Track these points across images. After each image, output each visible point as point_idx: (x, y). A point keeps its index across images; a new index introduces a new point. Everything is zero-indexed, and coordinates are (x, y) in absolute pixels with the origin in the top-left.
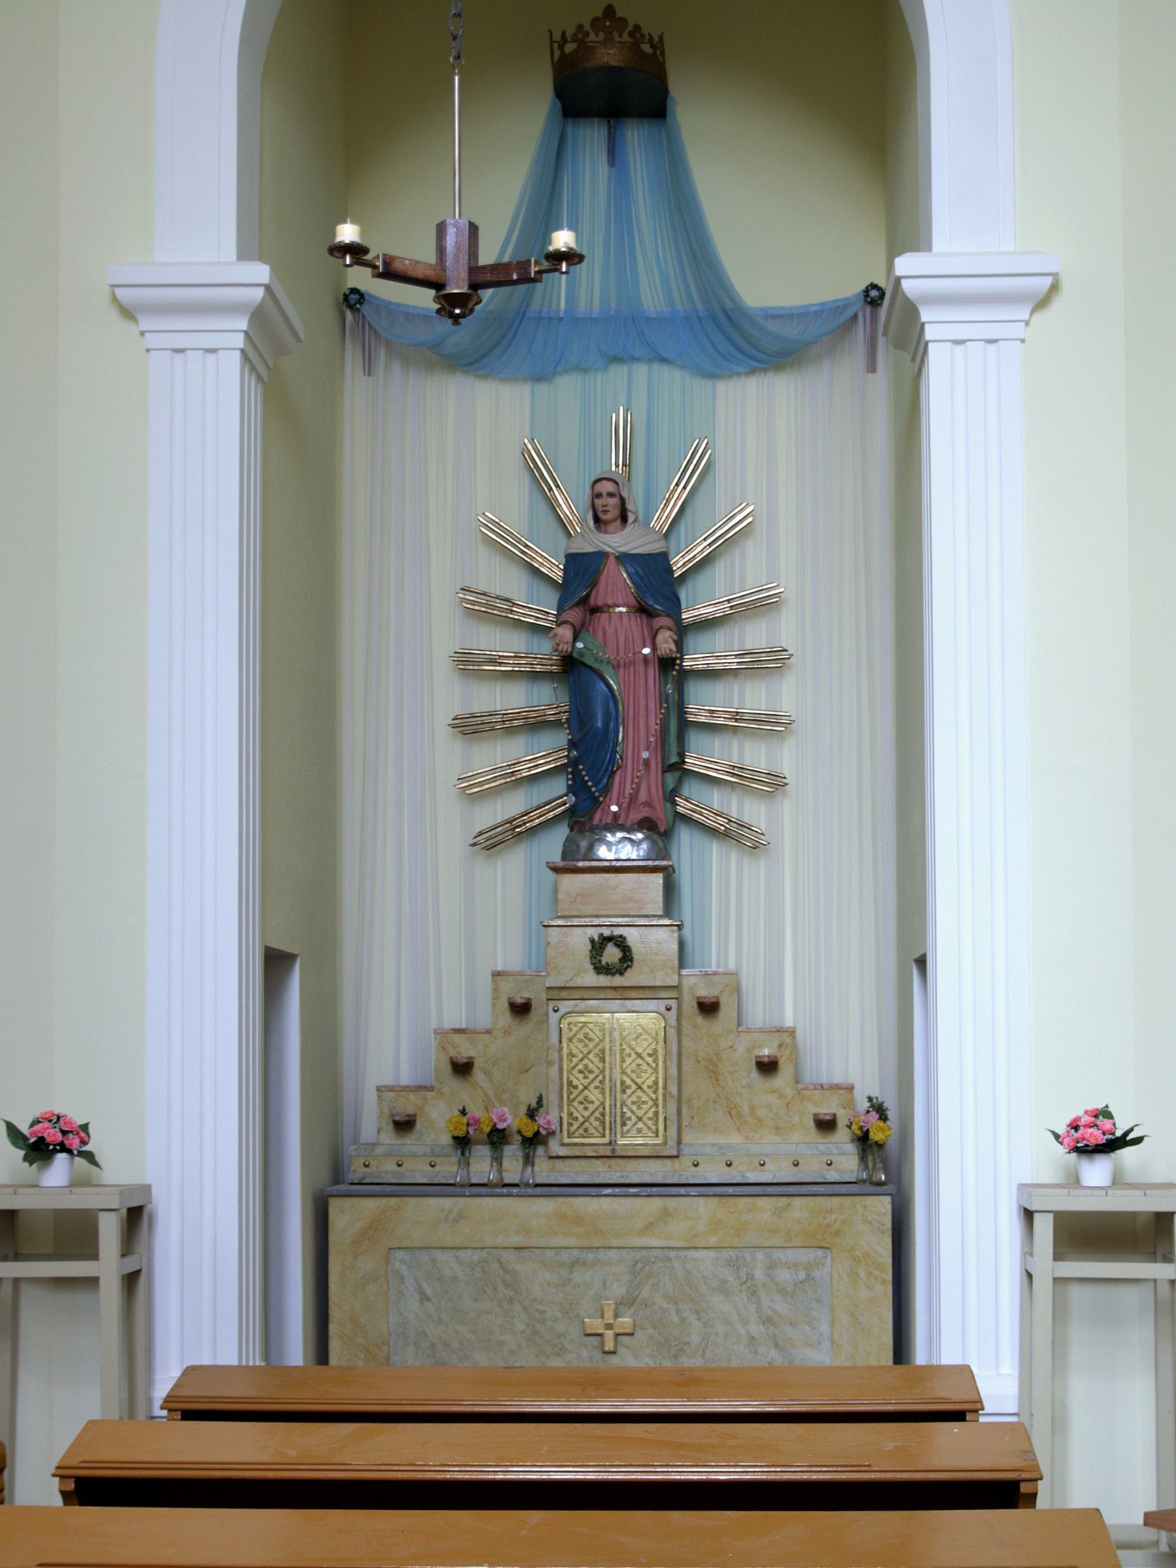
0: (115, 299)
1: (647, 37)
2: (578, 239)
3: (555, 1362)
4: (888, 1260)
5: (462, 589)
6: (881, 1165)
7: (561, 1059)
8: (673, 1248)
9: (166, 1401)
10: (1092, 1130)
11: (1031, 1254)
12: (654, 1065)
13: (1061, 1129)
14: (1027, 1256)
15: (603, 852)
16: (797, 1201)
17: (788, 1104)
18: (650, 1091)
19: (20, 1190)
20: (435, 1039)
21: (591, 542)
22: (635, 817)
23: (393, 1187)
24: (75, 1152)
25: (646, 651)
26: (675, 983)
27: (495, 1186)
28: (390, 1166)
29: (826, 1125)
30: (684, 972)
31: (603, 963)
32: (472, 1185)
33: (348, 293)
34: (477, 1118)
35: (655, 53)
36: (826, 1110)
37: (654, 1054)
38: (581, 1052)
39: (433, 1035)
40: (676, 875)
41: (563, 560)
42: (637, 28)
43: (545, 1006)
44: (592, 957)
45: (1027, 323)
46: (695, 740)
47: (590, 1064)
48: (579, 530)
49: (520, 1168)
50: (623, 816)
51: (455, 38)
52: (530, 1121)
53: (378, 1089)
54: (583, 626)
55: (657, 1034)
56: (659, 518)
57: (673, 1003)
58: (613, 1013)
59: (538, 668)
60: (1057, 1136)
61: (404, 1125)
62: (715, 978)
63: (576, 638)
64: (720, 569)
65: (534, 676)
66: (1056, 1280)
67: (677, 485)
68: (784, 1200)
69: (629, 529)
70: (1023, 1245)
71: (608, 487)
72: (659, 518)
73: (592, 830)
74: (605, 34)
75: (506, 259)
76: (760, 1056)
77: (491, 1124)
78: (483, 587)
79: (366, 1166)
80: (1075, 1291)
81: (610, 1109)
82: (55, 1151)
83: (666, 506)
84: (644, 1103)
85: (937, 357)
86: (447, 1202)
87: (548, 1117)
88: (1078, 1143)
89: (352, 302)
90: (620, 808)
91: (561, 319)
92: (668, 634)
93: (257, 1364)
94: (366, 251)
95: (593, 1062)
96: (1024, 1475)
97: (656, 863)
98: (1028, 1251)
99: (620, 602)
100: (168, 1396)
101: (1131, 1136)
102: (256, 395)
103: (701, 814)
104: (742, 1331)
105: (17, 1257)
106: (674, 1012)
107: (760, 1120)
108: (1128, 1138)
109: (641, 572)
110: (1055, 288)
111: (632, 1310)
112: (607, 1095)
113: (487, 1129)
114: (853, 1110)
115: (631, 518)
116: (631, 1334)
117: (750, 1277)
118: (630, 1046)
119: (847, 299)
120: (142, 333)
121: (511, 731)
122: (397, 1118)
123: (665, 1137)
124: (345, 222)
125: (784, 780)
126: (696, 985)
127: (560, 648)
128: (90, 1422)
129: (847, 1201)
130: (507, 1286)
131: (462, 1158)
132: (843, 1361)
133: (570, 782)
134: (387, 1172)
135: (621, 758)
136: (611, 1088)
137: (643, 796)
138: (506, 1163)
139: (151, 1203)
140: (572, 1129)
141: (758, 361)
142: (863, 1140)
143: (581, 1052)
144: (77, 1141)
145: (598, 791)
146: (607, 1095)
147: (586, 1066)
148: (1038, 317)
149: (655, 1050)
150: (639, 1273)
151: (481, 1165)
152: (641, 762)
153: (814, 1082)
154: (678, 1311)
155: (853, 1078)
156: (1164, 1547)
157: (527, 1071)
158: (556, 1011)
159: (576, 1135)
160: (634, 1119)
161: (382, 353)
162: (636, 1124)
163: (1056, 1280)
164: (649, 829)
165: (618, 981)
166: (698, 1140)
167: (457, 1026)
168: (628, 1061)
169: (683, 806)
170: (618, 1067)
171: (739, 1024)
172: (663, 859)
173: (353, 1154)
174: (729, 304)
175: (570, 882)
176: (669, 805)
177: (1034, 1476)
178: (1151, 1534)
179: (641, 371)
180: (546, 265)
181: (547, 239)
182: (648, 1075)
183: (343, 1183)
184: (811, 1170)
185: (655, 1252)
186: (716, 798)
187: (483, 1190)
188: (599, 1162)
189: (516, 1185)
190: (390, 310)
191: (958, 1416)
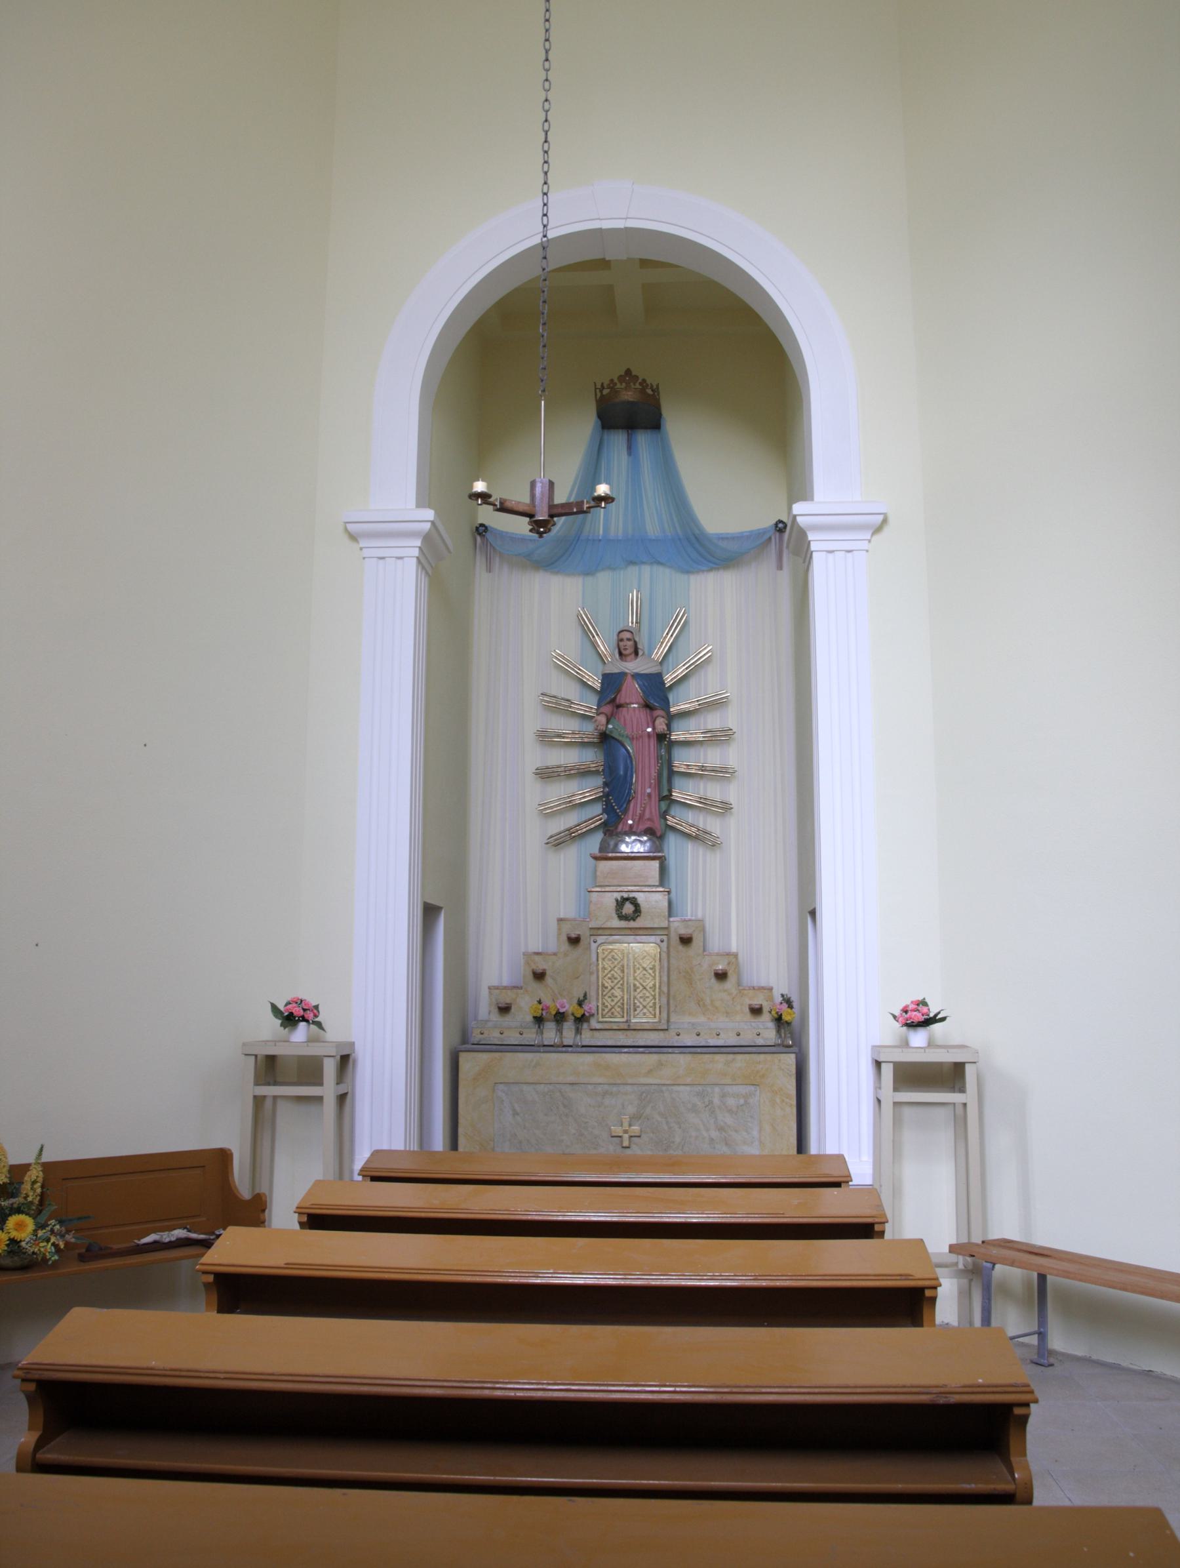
0: (346, 530)
1: (650, 385)
2: (611, 489)
3: (593, 1152)
4: (793, 1092)
5: (542, 694)
6: (789, 1035)
7: (598, 971)
8: (664, 1085)
9: (361, 1171)
10: (915, 1013)
11: (880, 1088)
12: (653, 975)
13: (897, 1013)
14: (878, 1089)
15: (623, 848)
16: (739, 1057)
17: (733, 998)
18: (651, 991)
19: (277, 1044)
20: (524, 958)
21: (617, 666)
22: (642, 827)
23: (498, 1047)
24: (311, 1022)
25: (649, 730)
26: (666, 926)
27: (558, 1046)
28: (496, 1034)
29: (756, 1011)
30: (671, 919)
31: (624, 913)
32: (544, 1046)
33: (478, 526)
34: (548, 1005)
35: (654, 394)
36: (757, 1001)
37: (653, 968)
38: (610, 966)
39: (522, 956)
40: (666, 862)
41: (601, 678)
42: (644, 381)
43: (588, 939)
44: (617, 910)
45: (869, 541)
46: (678, 782)
47: (615, 974)
48: (610, 660)
49: (573, 1036)
50: (635, 826)
51: (542, 381)
52: (579, 1007)
53: (489, 988)
54: (612, 715)
55: (655, 956)
56: (657, 653)
57: (665, 938)
58: (629, 943)
59: (586, 740)
60: (895, 1017)
61: (504, 1010)
62: (690, 923)
63: (608, 722)
64: (692, 682)
65: (583, 744)
66: (895, 1104)
67: (667, 634)
68: (731, 1056)
69: (638, 659)
70: (875, 1083)
71: (627, 635)
72: (657, 653)
73: (617, 834)
74: (626, 383)
75: (572, 500)
76: (717, 970)
77: (556, 1009)
78: (554, 693)
79: (482, 1034)
80: (907, 1112)
81: (627, 1001)
82: (299, 1021)
83: (661, 646)
84: (648, 997)
85: (818, 561)
86: (529, 1056)
87: (590, 1005)
88: (907, 1020)
89: (481, 531)
90: (633, 821)
91: (600, 540)
92: (662, 720)
93: (416, 1149)
94: (489, 496)
95: (617, 973)
96: (877, 1220)
97: (655, 854)
98: (878, 1085)
99: (634, 701)
100: (363, 1168)
101: (939, 1016)
102: (425, 583)
103: (682, 826)
104: (705, 1134)
105: (275, 1083)
106: (665, 944)
107: (717, 1008)
108: (937, 1018)
109: (646, 684)
110: (885, 521)
111: (640, 1122)
112: (625, 993)
113: (554, 1013)
114: (773, 1002)
115: (640, 653)
116: (639, 1137)
117: (711, 1102)
118: (639, 963)
119: (765, 528)
120: (361, 549)
121: (570, 776)
122: (500, 1005)
123: (660, 1018)
124: (478, 480)
125: (731, 806)
126: (678, 927)
127: (599, 728)
128: (317, 1181)
129: (769, 1057)
130: (565, 1106)
131: (539, 1030)
132: (766, 1152)
133: (604, 807)
134: (494, 1037)
135: (635, 793)
136: (627, 988)
137: (647, 815)
138: (565, 1033)
139: (354, 1052)
140: (604, 1013)
141: (715, 564)
142: (779, 1020)
143: (610, 966)
144: (312, 1015)
145: (620, 812)
146: (625, 993)
147: (613, 975)
148: (876, 538)
149: (654, 966)
150: (644, 1099)
151: (550, 1034)
152: (646, 794)
153: (749, 985)
154: (667, 1123)
155: (772, 982)
156: (961, 1266)
157: (577, 978)
158: (595, 942)
159: (607, 1016)
160: (641, 1006)
161: (497, 559)
162: (642, 1010)
163: (895, 1104)
164: (651, 834)
165: (632, 924)
166: (681, 1020)
167: (537, 951)
168: (638, 972)
169: (671, 821)
170: (632, 976)
171: (704, 950)
172: (659, 852)
173: (475, 1026)
174: (697, 532)
175: (604, 866)
176: (662, 821)
177: (883, 1220)
178: (953, 1258)
179: (646, 570)
180: (593, 504)
181: (594, 490)
182: (649, 981)
183: (468, 1043)
184: (747, 1038)
185: (653, 1087)
186: (690, 816)
187: (551, 1049)
188: (620, 1033)
189: (571, 1046)
190: (502, 535)
191: (837, 1185)
